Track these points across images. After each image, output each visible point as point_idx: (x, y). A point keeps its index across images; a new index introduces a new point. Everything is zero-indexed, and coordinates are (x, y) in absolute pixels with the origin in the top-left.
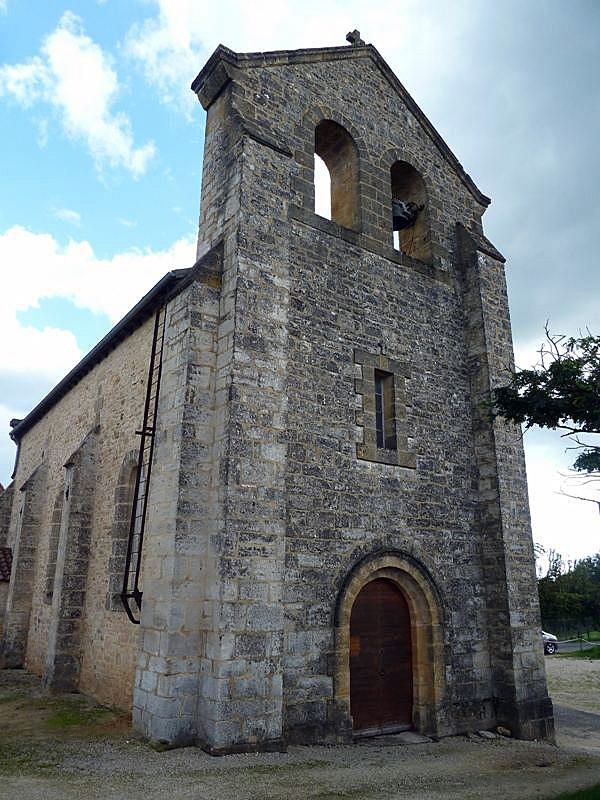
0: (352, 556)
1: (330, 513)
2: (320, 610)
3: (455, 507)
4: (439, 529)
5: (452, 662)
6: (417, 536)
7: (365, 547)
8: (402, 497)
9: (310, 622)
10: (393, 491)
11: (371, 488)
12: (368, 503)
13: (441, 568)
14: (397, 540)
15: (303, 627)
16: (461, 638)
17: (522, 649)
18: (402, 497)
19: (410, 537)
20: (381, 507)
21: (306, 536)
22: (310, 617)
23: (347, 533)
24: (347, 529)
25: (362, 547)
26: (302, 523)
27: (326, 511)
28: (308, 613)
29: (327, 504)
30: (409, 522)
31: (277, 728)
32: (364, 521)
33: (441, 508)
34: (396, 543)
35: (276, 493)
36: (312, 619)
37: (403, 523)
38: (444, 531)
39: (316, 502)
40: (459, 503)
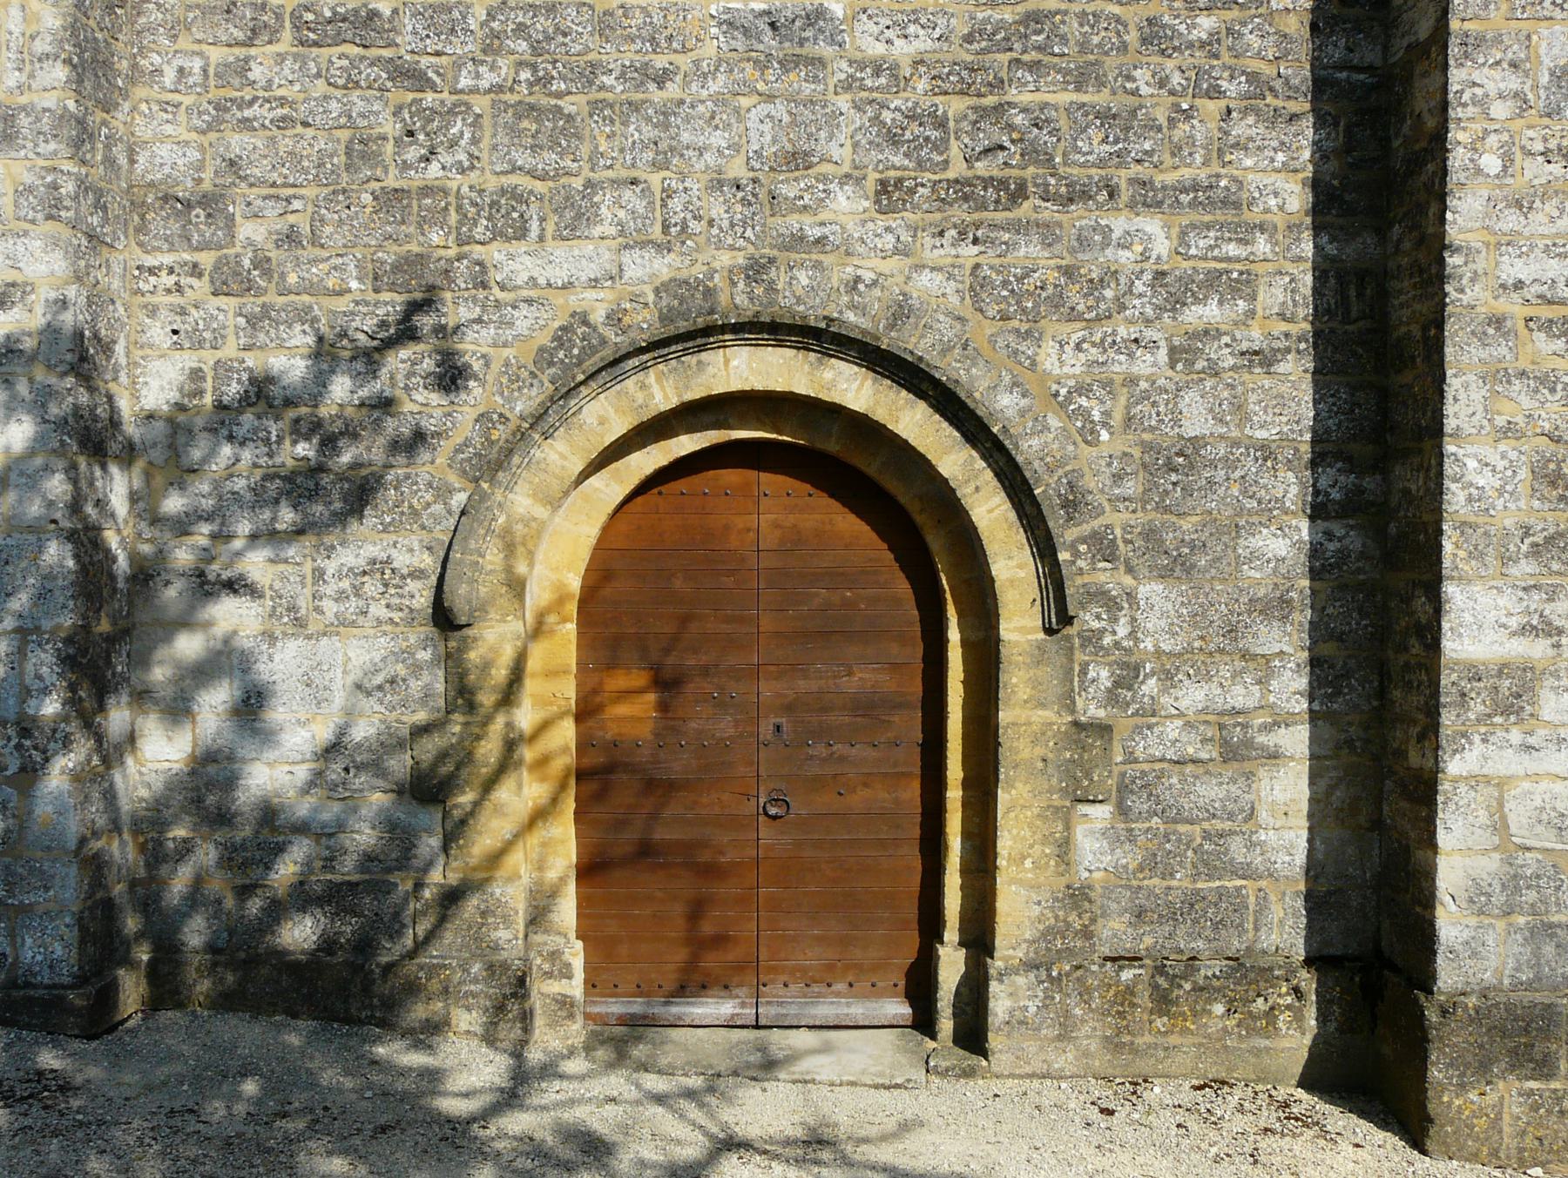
0: (544, 357)
1: (426, 191)
2: (378, 567)
3: (1213, 107)
4: (1080, 217)
5: (1124, 789)
6: (931, 256)
7: (614, 318)
8: (848, 85)
9: (330, 607)
10: (789, 64)
11: (660, 62)
12: (638, 130)
13: (1082, 389)
14: (803, 278)
15: (299, 623)
16: (1192, 696)
17: (1505, 762)
18: (848, 85)
19: (909, 273)
20: (718, 139)
21: (312, 289)
22: (330, 589)
23: (515, 263)
24: (520, 247)
25: (598, 316)
26: (290, 238)
27: (414, 180)
28: (319, 574)
29: (412, 154)
30: (889, 194)
31: (59, 950)
32: (611, 211)
33: (1106, 116)
34: (800, 290)
35: (24, 121)
36: (341, 597)
37: (847, 204)
38: (1119, 224)
39: (362, 150)
40: (1231, 88)
